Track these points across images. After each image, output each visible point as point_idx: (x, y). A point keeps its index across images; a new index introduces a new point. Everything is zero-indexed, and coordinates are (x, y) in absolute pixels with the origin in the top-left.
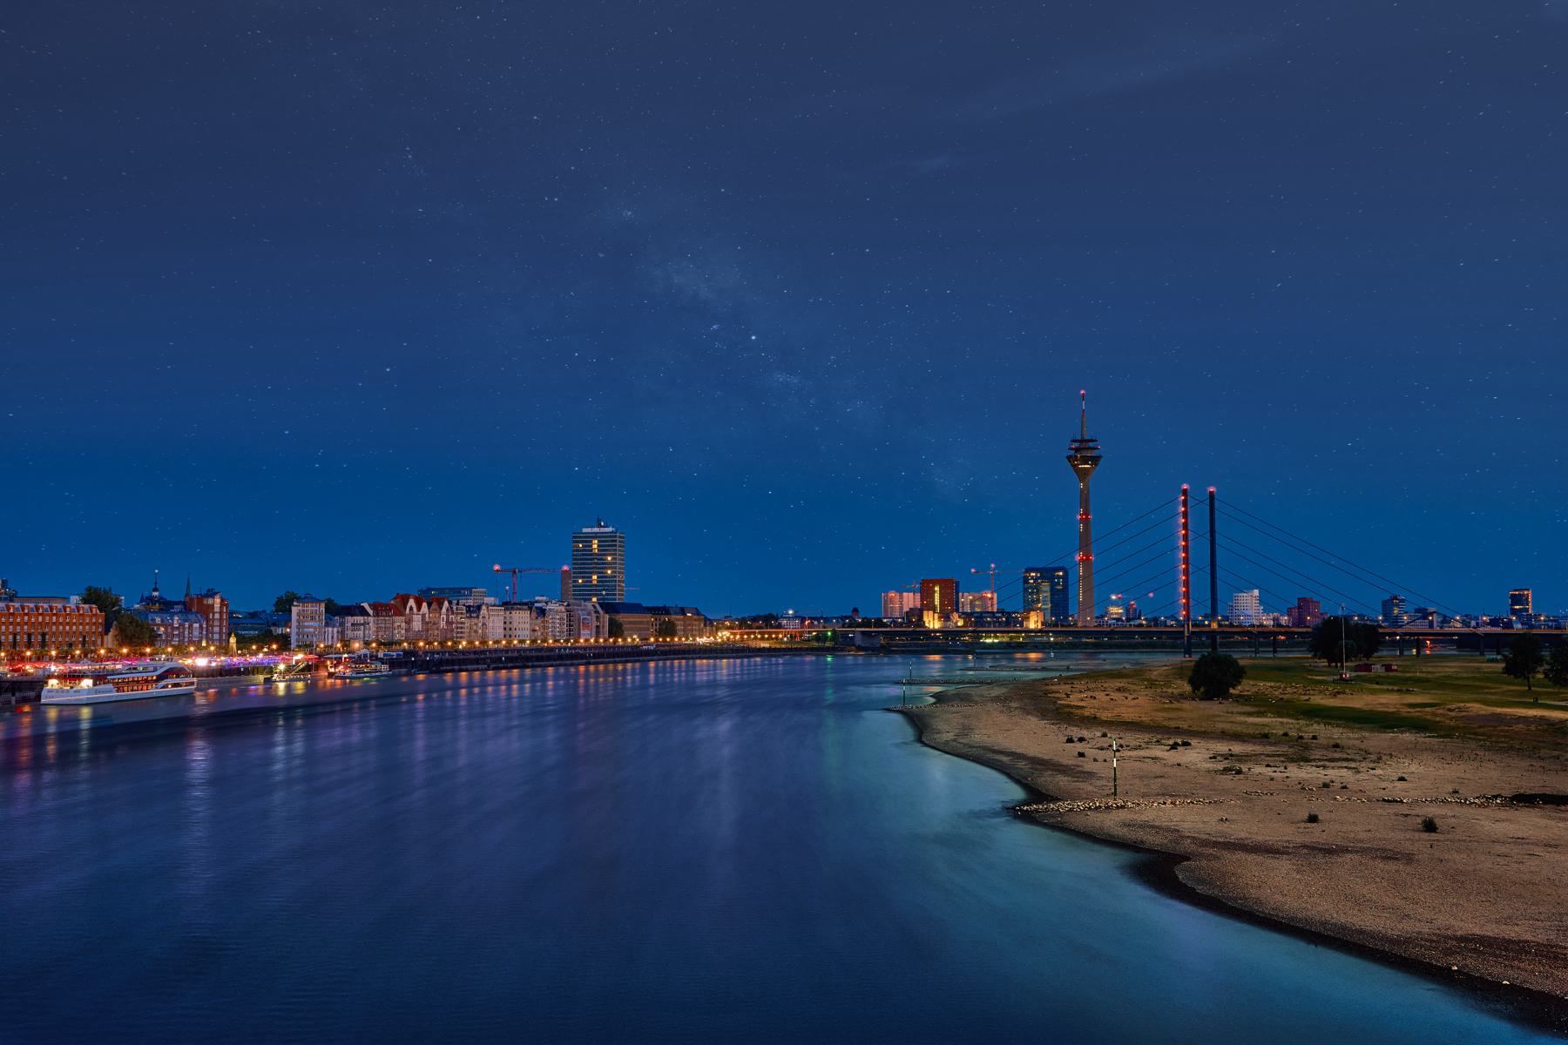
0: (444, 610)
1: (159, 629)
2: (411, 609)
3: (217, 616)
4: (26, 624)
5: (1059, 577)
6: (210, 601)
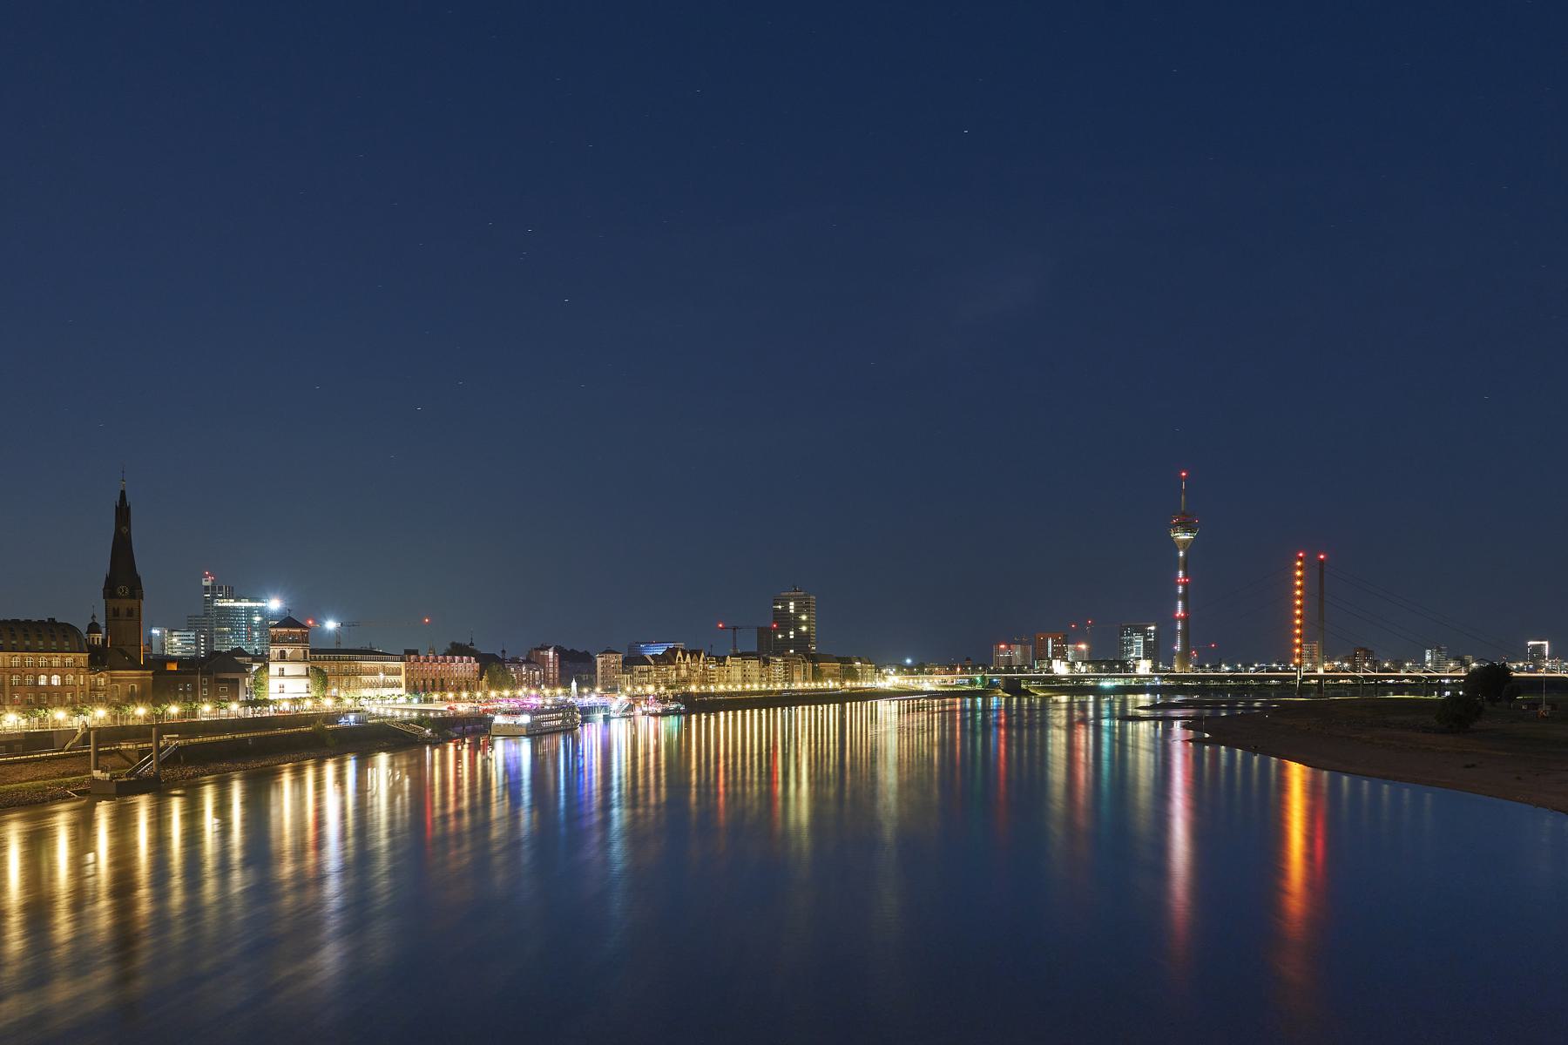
0: (701, 661)
2: (679, 659)
3: (551, 666)
5: (1150, 631)
6: (546, 653)
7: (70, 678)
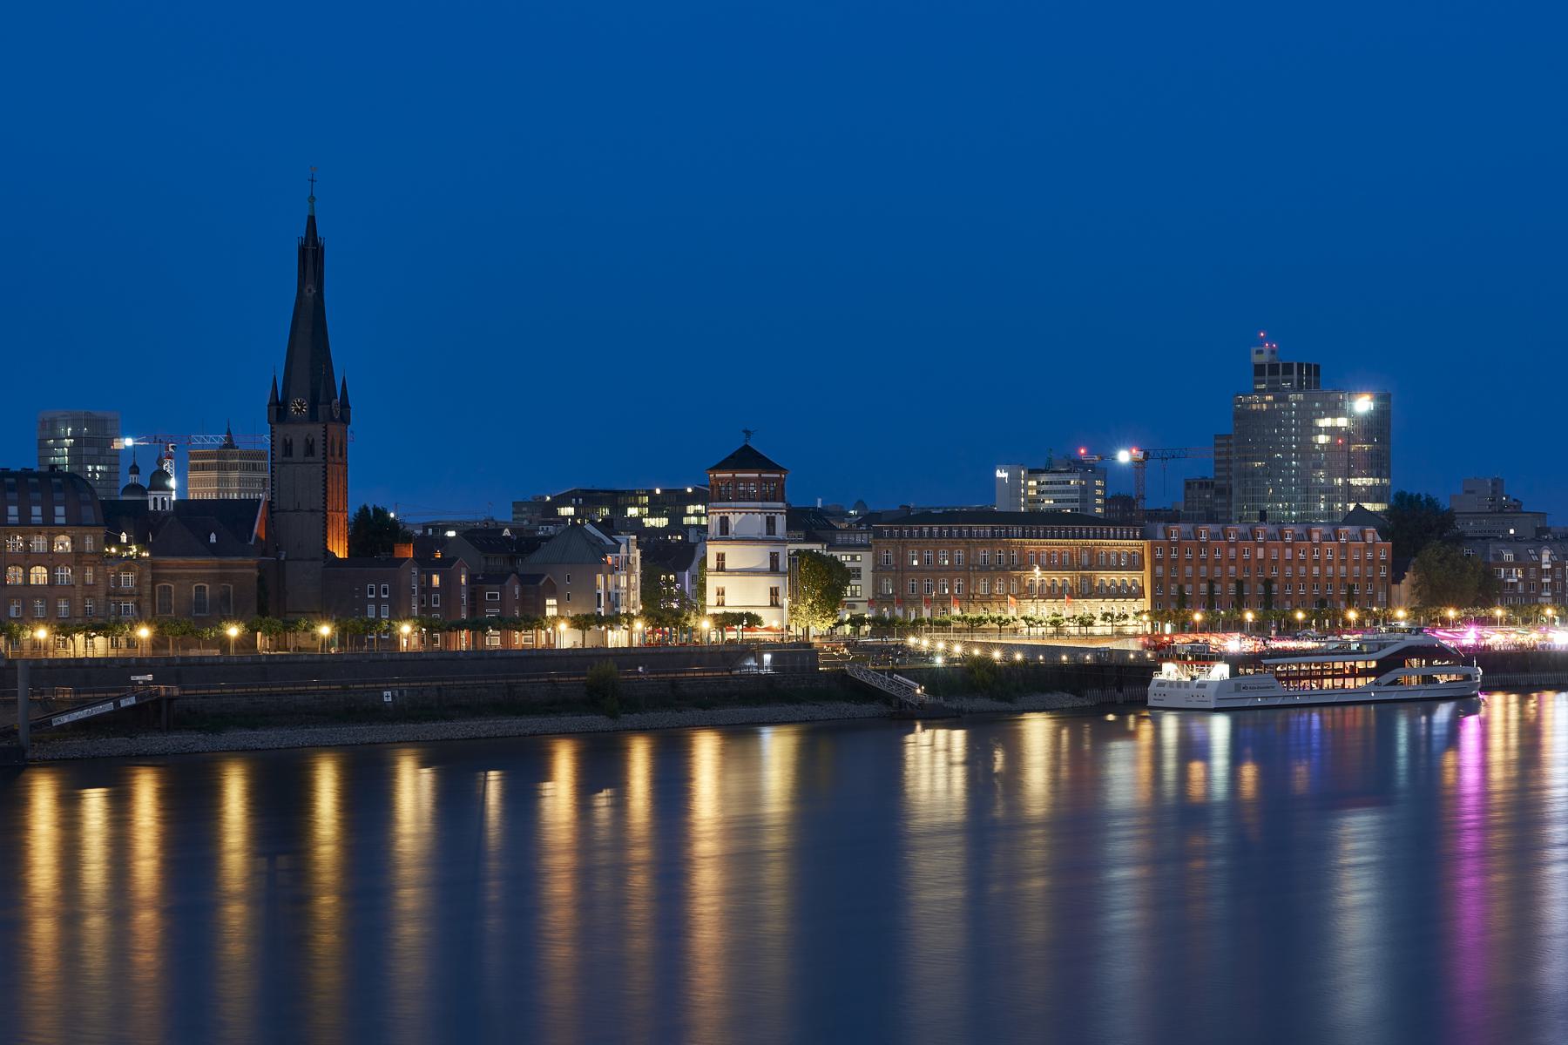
1: (1509, 574)
4: (1232, 562)
7: (65, 573)
